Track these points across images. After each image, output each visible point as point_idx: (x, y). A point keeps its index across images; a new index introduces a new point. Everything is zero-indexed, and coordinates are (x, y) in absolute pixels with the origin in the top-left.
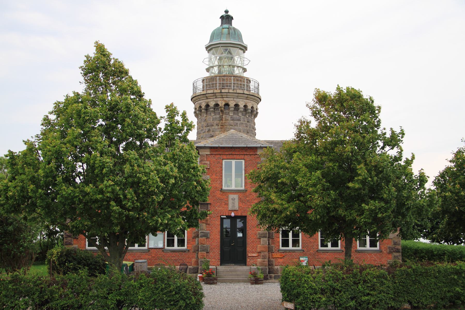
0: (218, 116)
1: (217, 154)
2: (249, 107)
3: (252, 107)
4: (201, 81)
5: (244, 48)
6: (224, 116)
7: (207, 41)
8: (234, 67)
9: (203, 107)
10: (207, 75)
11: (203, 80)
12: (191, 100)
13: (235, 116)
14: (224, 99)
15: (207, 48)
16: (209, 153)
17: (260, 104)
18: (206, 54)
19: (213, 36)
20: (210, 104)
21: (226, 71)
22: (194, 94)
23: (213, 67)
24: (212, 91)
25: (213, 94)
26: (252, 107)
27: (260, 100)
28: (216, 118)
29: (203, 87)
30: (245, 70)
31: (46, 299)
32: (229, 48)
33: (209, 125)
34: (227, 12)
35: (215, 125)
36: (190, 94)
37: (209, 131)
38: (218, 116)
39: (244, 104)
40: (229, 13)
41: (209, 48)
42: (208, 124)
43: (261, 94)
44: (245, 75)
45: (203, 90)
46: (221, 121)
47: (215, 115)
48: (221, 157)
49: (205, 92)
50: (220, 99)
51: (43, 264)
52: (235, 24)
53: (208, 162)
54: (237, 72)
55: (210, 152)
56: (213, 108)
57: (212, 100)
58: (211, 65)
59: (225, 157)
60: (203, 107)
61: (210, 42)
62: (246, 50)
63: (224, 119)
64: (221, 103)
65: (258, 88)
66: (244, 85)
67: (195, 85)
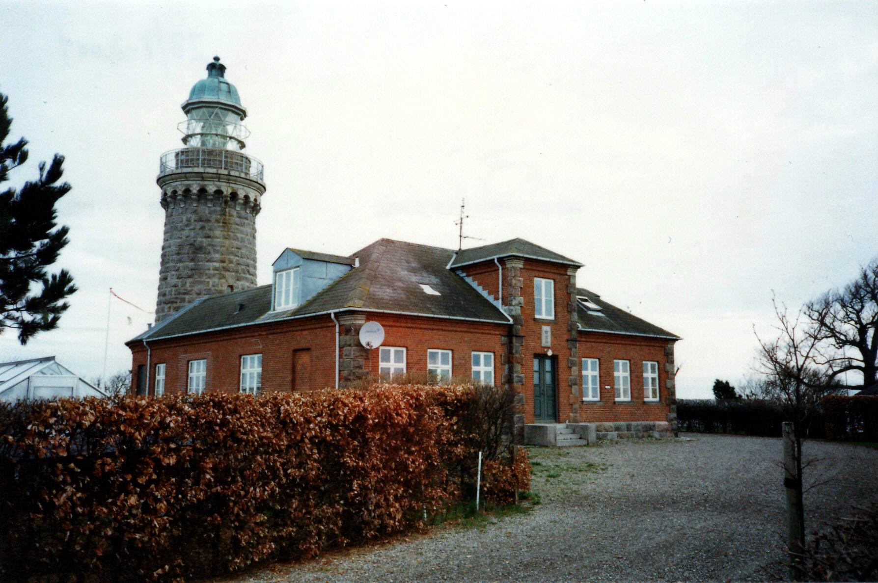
0: (219, 209)
1: (535, 270)
2: (252, 199)
3: (256, 200)
4: (174, 155)
5: (242, 114)
6: (227, 210)
7: (184, 97)
8: (224, 137)
9: (180, 192)
10: (182, 146)
11: (177, 155)
12: (158, 181)
13: (243, 213)
14: (231, 185)
15: (184, 108)
16: (521, 266)
17: (265, 195)
18: (183, 117)
19: (194, 91)
20: (191, 189)
21: (211, 142)
22: (161, 172)
23: (191, 136)
24: (214, 171)
25: (215, 175)
26: (256, 200)
27: (263, 189)
28: (215, 211)
29: (177, 164)
30: (242, 145)
31: (363, 416)
32: (216, 110)
33: (203, 219)
34: (216, 68)
35: (213, 221)
36: (156, 172)
37: (203, 228)
38: (219, 209)
39: (244, 194)
40: (221, 62)
41: (188, 108)
42: (200, 218)
43: (267, 181)
44: (243, 151)
45: (177, 168)
46: (224, 217)
47: (214, 206)
48: (534, 273)
49: (179, 171)
50: (224, 184)
51: (430, 370)
52: (228, 76)
53: (522, 279)
54: (232, 146)
55: (524, 265)
56: (212, 195)
57: (212, 183)
58: (190, 133)
59: (537, 274)
60: (180, 192)
61: (191, 98)
62: (245, 116)
64: (226, 190)
65: (261, 173)
66: (221, 161)
67: (164, 160)
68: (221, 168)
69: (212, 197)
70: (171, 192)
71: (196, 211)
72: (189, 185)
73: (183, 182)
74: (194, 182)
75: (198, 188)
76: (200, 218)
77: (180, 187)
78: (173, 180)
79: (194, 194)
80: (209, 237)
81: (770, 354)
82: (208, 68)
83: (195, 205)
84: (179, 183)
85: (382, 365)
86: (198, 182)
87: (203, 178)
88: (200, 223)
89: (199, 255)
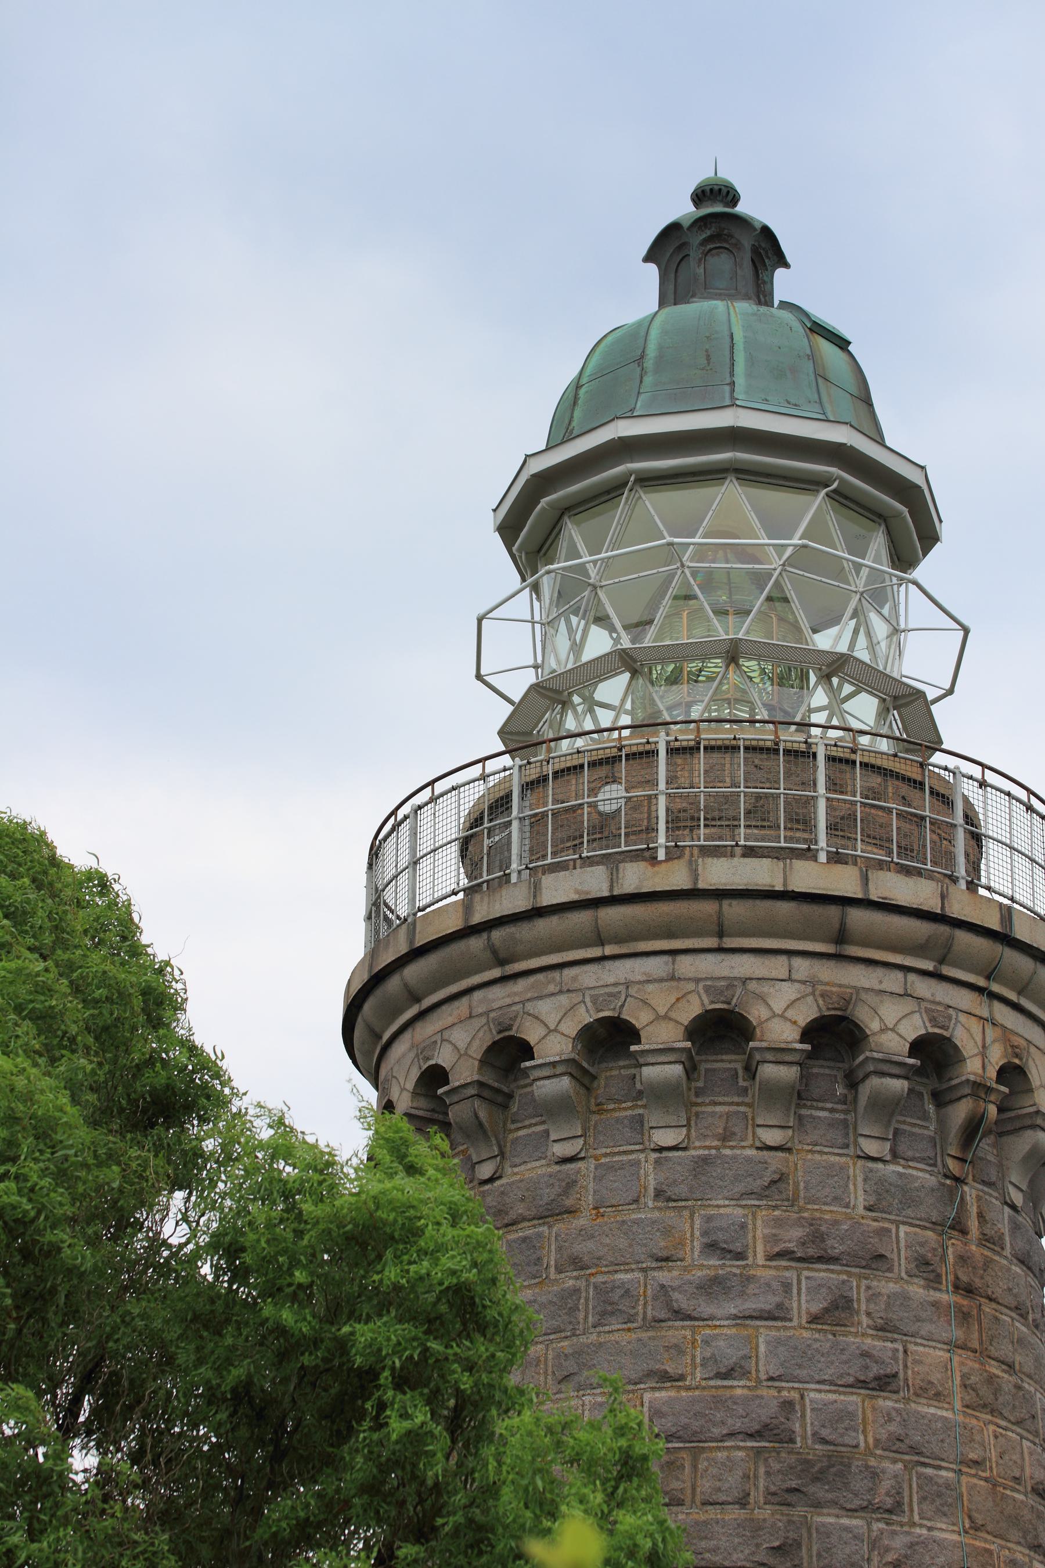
20: (756, 1013)
25: (922, 929)
33: (835, 1247)
35: (902, 1263)
42: (817, 1237)
62: (929, 538)
63: (973, 1224)
68: (809, 854)
69: (899, 1086)
70: (571, 1027)
71: (781, 1179)
72: (850, 998)
73: (686, 965)
74: (777, 966)
75: (806, 1013)
76: (817, 1237)
77: (661, 999)
78: (601, 941)
79: (779, 1054)
80: (884, 1383)
81: (168, 963)
82: (693, 200)
83: (772, 1137)
84: (656, 966)
85: (194, 1128)
86: (802, 967)
87: (841, 937)
88: (821, 1274)
89: (827, 1519)
